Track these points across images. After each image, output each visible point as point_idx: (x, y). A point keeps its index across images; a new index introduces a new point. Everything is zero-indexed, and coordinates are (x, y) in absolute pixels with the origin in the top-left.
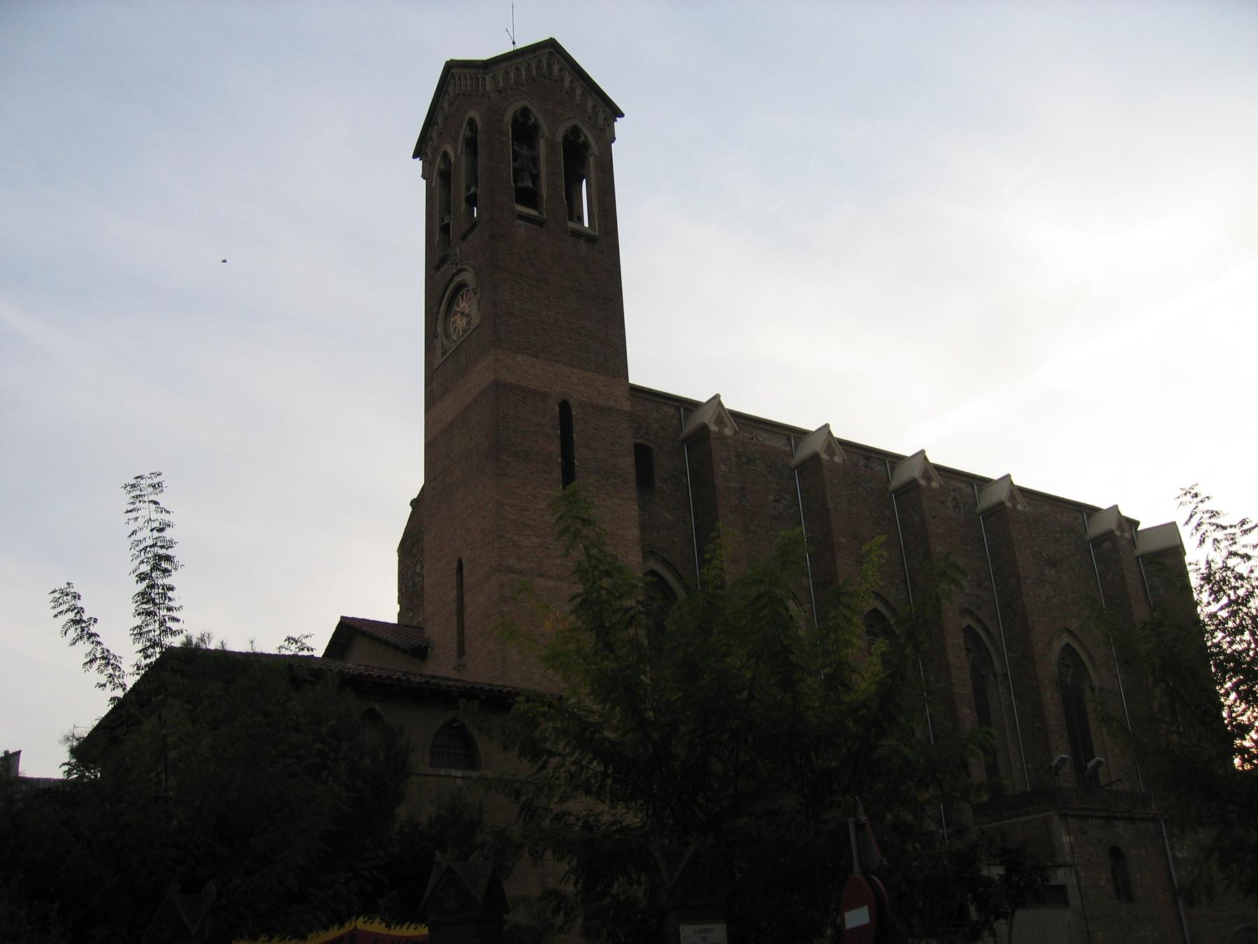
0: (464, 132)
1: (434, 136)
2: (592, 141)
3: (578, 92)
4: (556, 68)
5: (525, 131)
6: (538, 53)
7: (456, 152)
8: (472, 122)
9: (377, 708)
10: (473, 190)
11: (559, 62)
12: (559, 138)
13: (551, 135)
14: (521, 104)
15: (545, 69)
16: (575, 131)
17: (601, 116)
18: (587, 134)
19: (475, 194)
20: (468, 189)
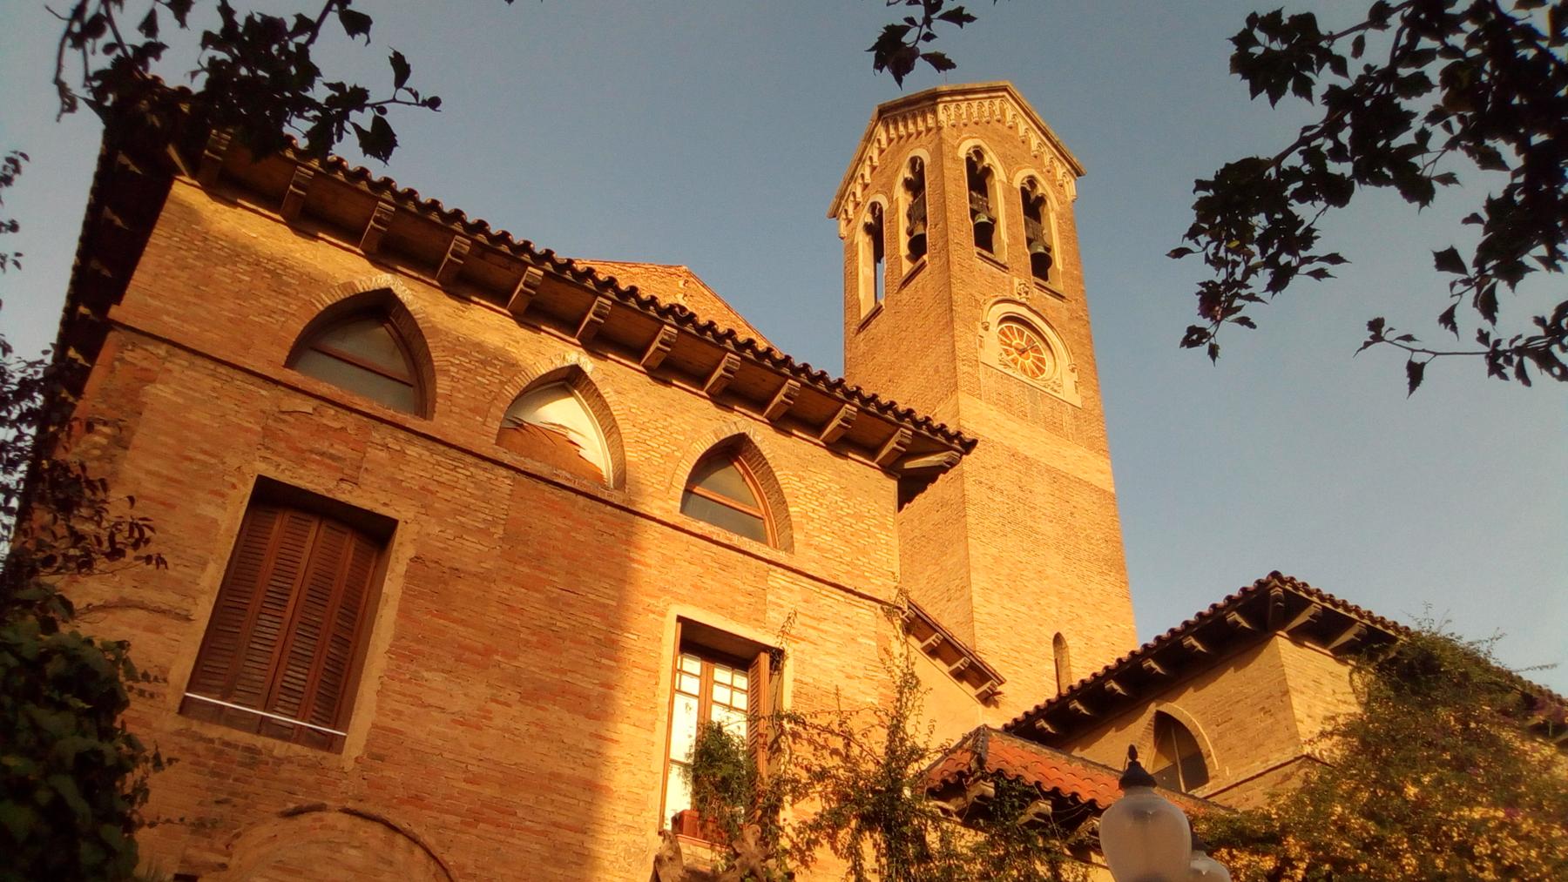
5: (979, 178)
12: (1017, 184)
15: (998, 112)
16: (1032, 181)
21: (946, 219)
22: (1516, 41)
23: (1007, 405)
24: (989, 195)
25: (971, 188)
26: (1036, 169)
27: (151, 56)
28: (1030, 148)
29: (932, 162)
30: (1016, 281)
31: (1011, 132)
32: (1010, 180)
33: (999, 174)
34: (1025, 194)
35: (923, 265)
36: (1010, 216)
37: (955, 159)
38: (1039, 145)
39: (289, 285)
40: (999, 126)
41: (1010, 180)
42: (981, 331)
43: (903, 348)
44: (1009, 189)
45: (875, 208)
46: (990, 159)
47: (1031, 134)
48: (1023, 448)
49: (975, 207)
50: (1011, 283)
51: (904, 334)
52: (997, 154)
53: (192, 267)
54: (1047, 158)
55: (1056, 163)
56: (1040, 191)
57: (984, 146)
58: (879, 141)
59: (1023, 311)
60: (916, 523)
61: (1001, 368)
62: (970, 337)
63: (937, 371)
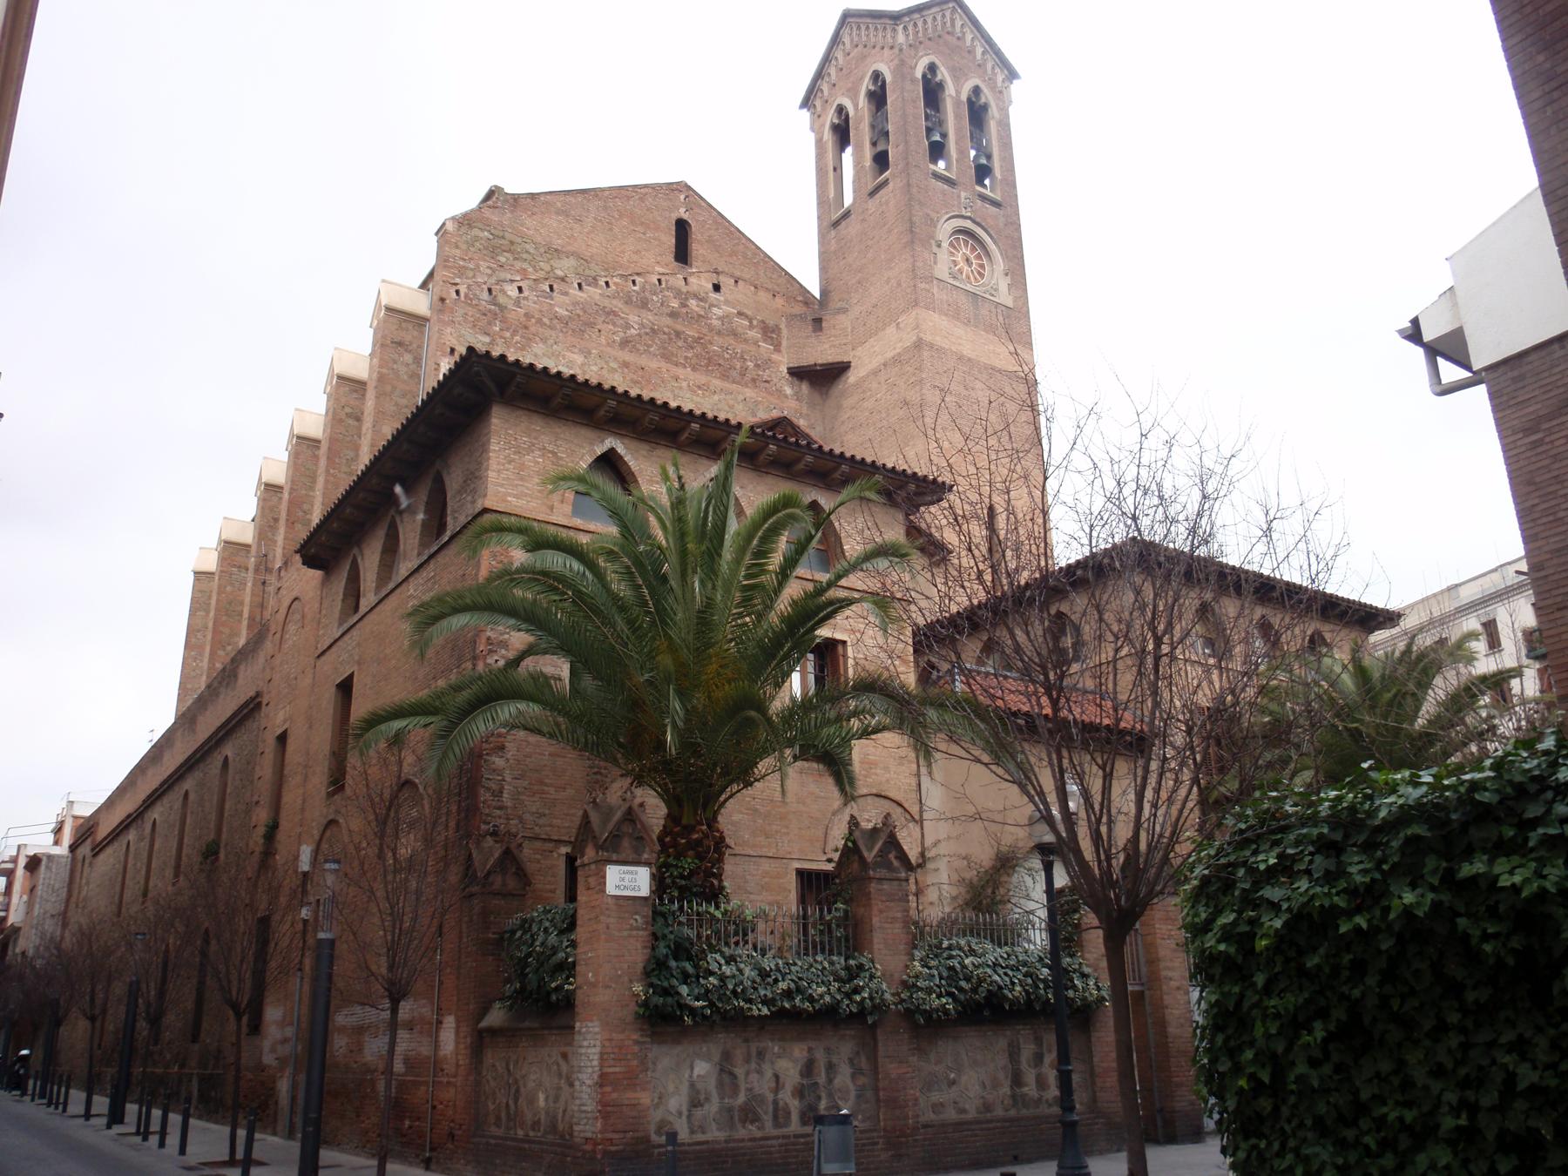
0: (866, 84)
1: (825, 88)
2: (993, 104)
3: (979, 50)
4: (958, 23)
5: (932, 93)
6: (925, 13)
7: (856, 106)
8: (877, 76)
9: (621, 450)
10: (880, 148)
11: (961, 18)
12: (964, 97)
13: (955, 93)
14: (932, 58)
15: (949, 24)
16: (976, 91)
17: (1000, 78)
18: (987, 96)
19: (934, 159)
20: (874, 144)
21: (906, 142)
22: (1365, 765)
23: (955, 314)
24: (941, 109)
25: (927, 105)
26: (980, 77)
27: (1090, 1153)
28: (975, 57)
29: (893, 82)
30: (963, 194)
31: (959, 43)
32: (958, 92)
33: (950, 89)
34: (970, 102)
35: (885, 183)
36: (958, 130)
37: (914, 80)
38: (983, 53)
39: (562, 458)
40: (949, 38)
41: (958, 92)
42: (935, 249)
43: (869, 255)
44: (957, 102)
45: (841, 110)
46: (943, 74)
47: (976, 43)
48: (967, 351)
49: (930, 125)
50: (959, 196)
51: (870, 243)
52: (947, 68)
53: (513, 460)
54: (989, 66)
55: (997, 70)
56: (983, 100)
57: (938, 62)
58: (844, 44)
59: (968, 224)
60: (884, 415)
61: (951, 281)
62: (926, 255)
63: (899, 285)
